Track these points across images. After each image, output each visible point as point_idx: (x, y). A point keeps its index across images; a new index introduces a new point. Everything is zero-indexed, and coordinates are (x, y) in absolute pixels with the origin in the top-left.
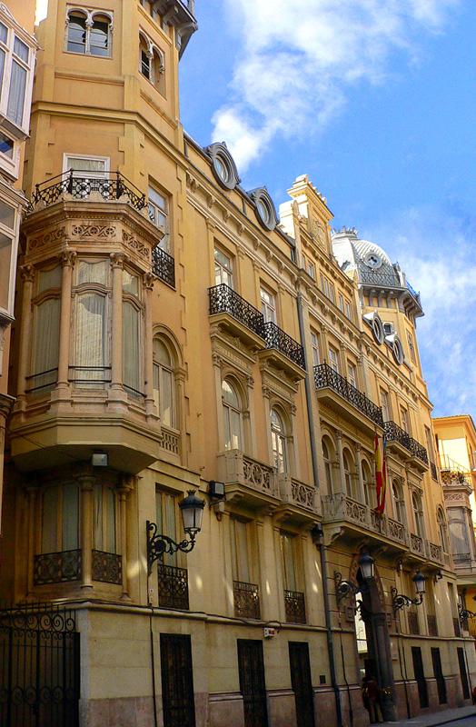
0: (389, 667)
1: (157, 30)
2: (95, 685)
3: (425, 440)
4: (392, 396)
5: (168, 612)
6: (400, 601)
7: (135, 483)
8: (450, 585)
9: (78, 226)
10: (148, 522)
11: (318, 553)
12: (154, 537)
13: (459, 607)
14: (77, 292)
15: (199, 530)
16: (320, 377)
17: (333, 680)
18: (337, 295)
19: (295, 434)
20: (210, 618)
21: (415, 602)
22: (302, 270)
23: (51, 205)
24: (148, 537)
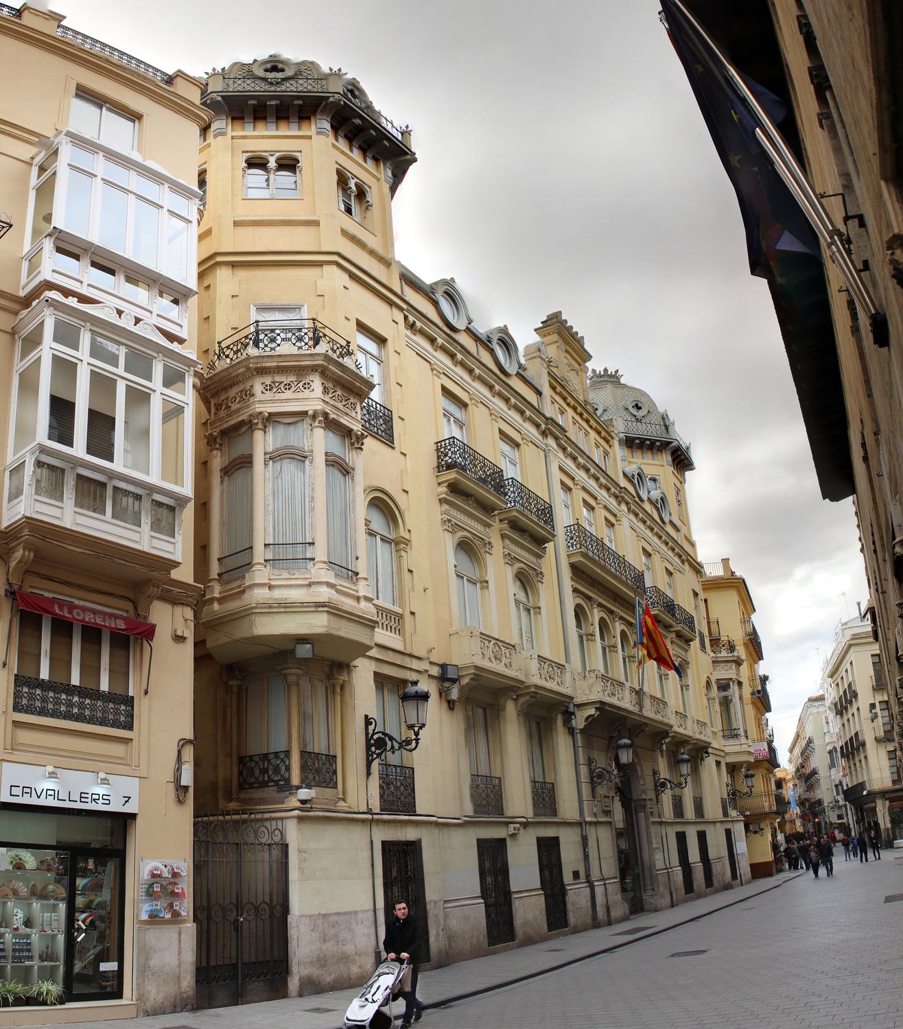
0: (651, 855)
2: (303, 901)
6: (663, 785)
7: (349, 673)
8: (718, 763)
9: (268, 382)
10: (366, 716)
11: (571, 738)
12: (374, 734)
13: (727, 786)
14: (270, 459)
15: (424, 725)
16: (572, 538)
17: (588, 876)
20: (440, 820)
21: (679, 785)
23: (237, 361)
24: (367, 734)
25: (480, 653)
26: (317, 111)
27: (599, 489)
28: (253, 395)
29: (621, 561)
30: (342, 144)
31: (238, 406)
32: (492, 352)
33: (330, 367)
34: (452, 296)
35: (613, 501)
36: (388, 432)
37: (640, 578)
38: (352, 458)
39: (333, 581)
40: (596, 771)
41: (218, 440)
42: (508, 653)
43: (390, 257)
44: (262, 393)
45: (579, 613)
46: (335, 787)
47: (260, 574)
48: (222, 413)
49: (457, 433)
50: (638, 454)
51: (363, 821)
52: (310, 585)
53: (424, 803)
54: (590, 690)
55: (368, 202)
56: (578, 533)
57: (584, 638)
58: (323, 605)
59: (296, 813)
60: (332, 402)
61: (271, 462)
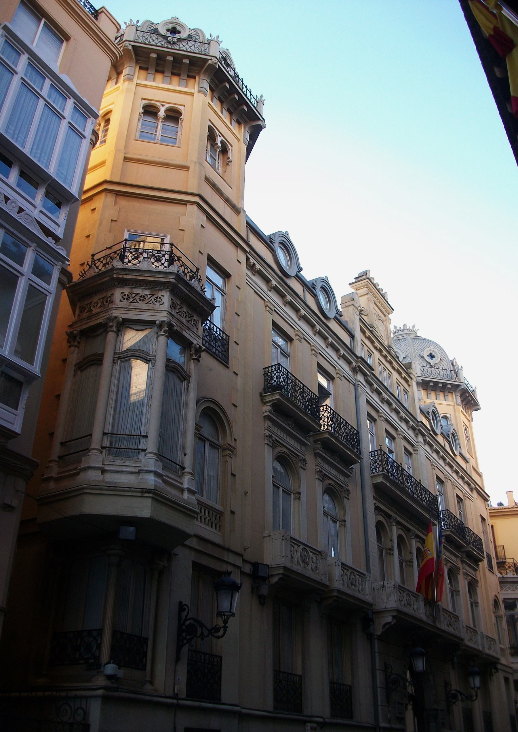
1: (226, 125)
3: (481, 530)
4: (448, 485)
5: (196, 704)
6: (455, 696)
8: (506, 680)
14: (119, 358)
18: (396, 385)
19: (348, 519)
20: (244, 711)
21: (470, 698)
22: (361, 358)
24: (180, 619)
25: (289, 556)
26: (200, 71)
27: (399, 422)
28: (112, 302)
29: (418, 485)
30: (217, 106)
31: (98, 310)
32: (315, 296)
33: (180, 285)
34: (287, 246)
35: (411, 432)
36: (224, 353)
37: (434, 501)
38: (192, 368)
39: (160, 471)
40: (392, 677)
41: (78, 339)
42: (314, 558)
43: (240, 206)
44: (120, 301)
45: (380, 527)
46: (144, 668)
47: (95, 459)
48: (85, 315)
49: (281, 360)
50: (433, 394)
51: (168, 706)
52: (140, 472)
53: (229, 692)
54: (388, 599)
55: (229, 158)
56: (381, 456)
57: (384, 552)
58: (148, 491)
59: (100, 692)
60: (178, 316)
61: (119, 362)
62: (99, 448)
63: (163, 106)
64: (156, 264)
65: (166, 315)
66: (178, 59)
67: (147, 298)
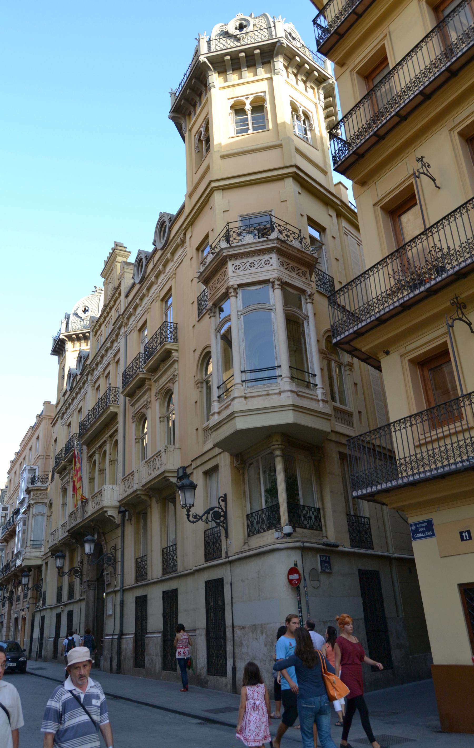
39: (294, 389)
62: (241, 382)
63: (247, 98)
64: (238, 238)
65: (276, 272)
66: (249, 53)
67: (263, 263)
